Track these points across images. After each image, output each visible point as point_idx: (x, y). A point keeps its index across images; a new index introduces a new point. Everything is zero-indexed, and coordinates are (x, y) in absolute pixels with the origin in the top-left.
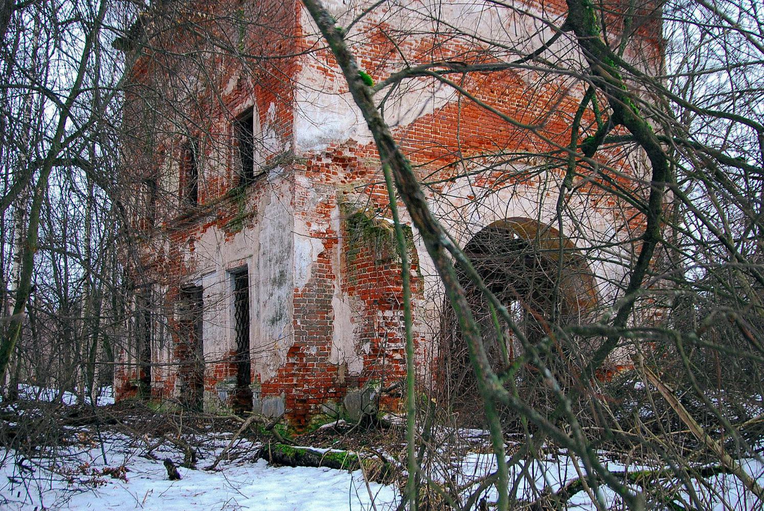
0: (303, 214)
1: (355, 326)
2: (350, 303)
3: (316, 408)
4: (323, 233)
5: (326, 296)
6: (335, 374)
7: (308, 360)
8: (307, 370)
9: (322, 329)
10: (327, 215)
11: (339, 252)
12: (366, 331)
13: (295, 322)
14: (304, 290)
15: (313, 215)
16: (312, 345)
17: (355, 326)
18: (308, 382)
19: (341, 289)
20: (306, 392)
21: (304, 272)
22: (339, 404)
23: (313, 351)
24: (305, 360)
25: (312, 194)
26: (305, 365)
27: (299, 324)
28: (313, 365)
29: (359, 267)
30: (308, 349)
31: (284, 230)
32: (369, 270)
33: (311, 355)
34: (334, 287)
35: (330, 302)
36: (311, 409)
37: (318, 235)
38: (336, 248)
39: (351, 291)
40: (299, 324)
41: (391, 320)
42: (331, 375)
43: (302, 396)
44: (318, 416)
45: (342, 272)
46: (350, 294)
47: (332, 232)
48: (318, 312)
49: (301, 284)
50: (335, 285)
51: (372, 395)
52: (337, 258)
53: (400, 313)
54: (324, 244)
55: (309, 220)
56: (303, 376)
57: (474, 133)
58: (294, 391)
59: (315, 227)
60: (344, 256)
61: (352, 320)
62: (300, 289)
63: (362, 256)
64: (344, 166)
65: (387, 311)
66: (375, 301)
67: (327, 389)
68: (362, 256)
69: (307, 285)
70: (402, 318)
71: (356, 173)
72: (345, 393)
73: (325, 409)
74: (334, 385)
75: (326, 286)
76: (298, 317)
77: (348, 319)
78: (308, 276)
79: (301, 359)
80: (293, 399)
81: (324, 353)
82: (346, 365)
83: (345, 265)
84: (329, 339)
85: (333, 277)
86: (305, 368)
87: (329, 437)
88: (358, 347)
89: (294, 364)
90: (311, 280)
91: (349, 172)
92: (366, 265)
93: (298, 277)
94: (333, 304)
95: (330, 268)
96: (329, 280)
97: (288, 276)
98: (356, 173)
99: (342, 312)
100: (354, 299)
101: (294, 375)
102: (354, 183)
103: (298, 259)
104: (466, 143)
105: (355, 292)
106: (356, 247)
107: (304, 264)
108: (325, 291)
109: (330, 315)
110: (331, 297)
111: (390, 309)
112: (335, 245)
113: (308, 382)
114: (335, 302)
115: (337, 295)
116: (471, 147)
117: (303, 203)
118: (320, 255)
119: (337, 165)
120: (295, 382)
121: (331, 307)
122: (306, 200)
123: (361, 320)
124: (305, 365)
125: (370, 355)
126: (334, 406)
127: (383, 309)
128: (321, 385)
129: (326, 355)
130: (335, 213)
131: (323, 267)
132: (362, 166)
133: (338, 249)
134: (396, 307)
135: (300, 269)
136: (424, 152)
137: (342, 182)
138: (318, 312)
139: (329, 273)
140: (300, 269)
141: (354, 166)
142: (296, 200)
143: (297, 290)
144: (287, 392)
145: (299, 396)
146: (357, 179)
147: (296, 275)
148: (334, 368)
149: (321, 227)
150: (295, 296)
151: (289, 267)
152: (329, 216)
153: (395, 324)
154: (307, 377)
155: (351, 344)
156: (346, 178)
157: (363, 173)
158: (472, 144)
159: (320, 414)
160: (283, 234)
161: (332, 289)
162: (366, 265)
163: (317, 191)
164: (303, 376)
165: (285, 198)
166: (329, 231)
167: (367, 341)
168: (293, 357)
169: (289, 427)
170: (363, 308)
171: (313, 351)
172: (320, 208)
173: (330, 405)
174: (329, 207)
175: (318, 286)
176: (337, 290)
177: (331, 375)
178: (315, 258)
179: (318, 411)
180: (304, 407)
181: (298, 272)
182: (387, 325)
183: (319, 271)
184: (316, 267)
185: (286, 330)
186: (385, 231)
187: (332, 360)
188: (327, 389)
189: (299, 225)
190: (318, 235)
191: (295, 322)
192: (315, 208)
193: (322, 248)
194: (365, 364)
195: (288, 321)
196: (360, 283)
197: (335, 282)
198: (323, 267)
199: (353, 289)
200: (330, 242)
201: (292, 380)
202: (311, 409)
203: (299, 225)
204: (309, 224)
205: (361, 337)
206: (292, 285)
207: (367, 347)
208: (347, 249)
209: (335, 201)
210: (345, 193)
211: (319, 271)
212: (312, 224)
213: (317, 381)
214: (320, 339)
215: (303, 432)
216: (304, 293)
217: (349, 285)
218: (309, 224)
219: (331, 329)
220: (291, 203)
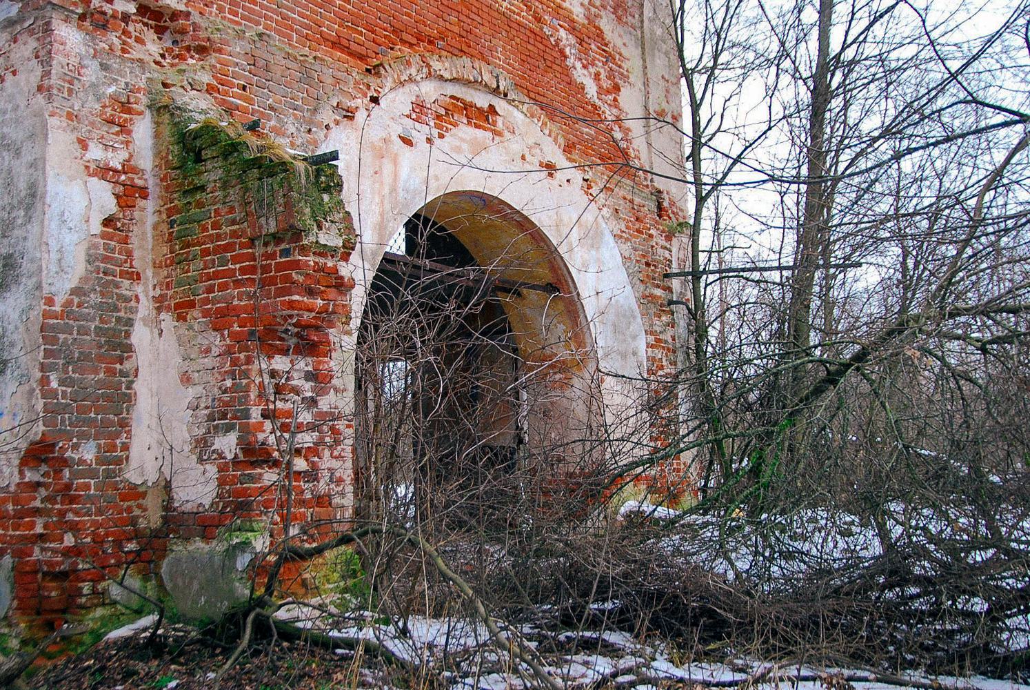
0: (70, 116)
1: (192, 392)
2: (179, 338)
3: (94, 592)
4: (115, 171)
5: (119, 320)
6: (139, 506)
7: (76, 475)
8: (73, 500)
9: (109, 398)
10: (124, 129)
11: (151, 219)
12: (227, 404)
13: (44, 381)
14: (69, 303)
15: (92, 124)
16: (84, 436)
17: (192, 392)
18: (74, 528)
19: (152, 305)
20: (67, 552)
21: (69, 259)
22: (146, 578)
23: (88, 452)
24: (66, 473)
25: (92, 73)
26: (68, 487)
27: (54, 384)
28: (88, 487)
29: (206, 252)
30: (75, 447)
31: (18, 153)
32: (235, 260)
33: (82, 461)
34: (137, 299)
35: (128, 335)
36: (81, 595)
37: (104, 172)
38: (143, 210)
39: (181, 310)
40: (54, 384)
41: (288, 379)
42: (129, 510)
43: (58, 564)
44: (99, 612)
45: (156, 266)
46: (181, 318)
47: (134, 170)
48: (100, 358)
49: (62, 286)
50: (141, 296)
51: (243, 561)
52: (144, 233)
53: (304, 364)
54: (117, 196)
55: (83, 134)
56: (62, 514)
57: (408, 15)
58: (37, 550)
59: (96, 153)
60: (164, 228)
61: (186, 379)
62: (59, 300)
63: (216, 226)
64: (160, 31)
65: (277, 357)
66: (252, 333)
67: (118, 544)
68: (216, 226)
69: (75, 291)
70: (309, 376)
71: (188, 49)
72: (163, 552)
73: (115, 591)
74: (137, 535)
75: (120, 297)
76: (53, 368)
77: (174, 375)
78: (77, 268)
79: (58, 472)
80: (36, 572)
81: (114, 457)
82: (168, 486)
83: (165, 250)
84: (124, 424)
85: (136, 277)
86: (67, 494)
87: (141, 667)
88: (202, 446)
89: (38, 484)
90: (84, 279)
91: (169, 44)
92: (227, 248)
93: (54, 268)
94: (134, 340)
95: (129, 254)
96: (126, 283)
97: (26, 266)
98: (188, 49)
99: (157, 359)
100: (191, 328)
101: (37, 512)
102: (184, 67)
103: (54, 225)
104: (394, 32)
105: (196, 313)
106: (200, 205)
107: (70, 239)
108: (116, 309)
109: (127, 365)
110: (130, 323)
111: (284, 352)
112: (141, 203)
113: (74, 528)
114: (141, 336)
115: (144, 320)
116: (404, 42)
117: (70, 91)
118: (108, 222)
119: (145, 24)
120: (39, 529)
121: (129, 348)
122: (77, 85)
123: (209, 378)
124: (68, 487)
125: (236, 462)
126: (134, 582)
127: (271, 352)
128: (107, 535)
129: (118, 461)
130: (143, 129)
131: (113, 251)
132: (202, 34)
133: (148, 213)
134: (299, 351)
135: (60, 251)
136: (321, 33)
137: (157, 63)
138: (100, 358)
139: (126, 267)
140: (60, 251)
141: (183, 32)
142: (54, 80)
143: (50, 301)
144: (20, 554)
145: (50, 564)
146: (190, 61)
147: (49, 263)
148: (135, 493)
149: (110, 155)
150: (46, 315)
151: (29, 244)
152: (129, 133)
153: (296, 391)
154: (70, 516)
155: (182, 434)
156: (163, 56)
157: (202, 51)
158: (405, 36)
159: (104, 604)
160: (16, 163)
161: (133, 304)
162: (227, 248)
163: (105, 67)
164: (62, 514)
165: (21, 77)
166: (128, 168)
167: (229, 429)
168: (35, 468)
169: (24, 643)
170: (215, 351)
171: (88, 452)
172: (109, 110)
173: (128, 581)
174: (129, 111)
175: (103, 295)
176: (145, 308)
177: (129, 510)
178: (96, 228)
179: (101, 598)
180: (63, 590)
181: (54, 256)
182: (278, 390)
183: (105, 259)
184: (95, 246)
185: (20, 400)
186: (284, 166)
187: (132, 475)
188: (118, 544)
189: (60, 141)
190: (104, 172)
191: (44, 381)
192: (97, 106)
193: (111, 206)
194: (222, 482)
195: (23, 379)
196: (210, 290)
197: (139, 289)
198: (113, 251)
199: (191, 305)
200: (129, 195)
201: (32, 525)
202: (81, 595)
203: (60, 141)
204: (83, 144)
205: (211, 418)
206: (39, 287)
207: (228, 444)
208: (170, 212)
209: (144, 100)
210: (165, 85)
211: (105, 259)
212: (91, 145)
213: (98, 525)
214: (106, 423)
215: (62, 652)
216: (67, 313)
217: (176, 295)
218: (83, 144)
219: (129, 399)
220: (40, 88)
